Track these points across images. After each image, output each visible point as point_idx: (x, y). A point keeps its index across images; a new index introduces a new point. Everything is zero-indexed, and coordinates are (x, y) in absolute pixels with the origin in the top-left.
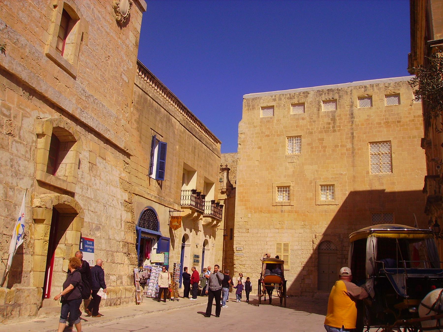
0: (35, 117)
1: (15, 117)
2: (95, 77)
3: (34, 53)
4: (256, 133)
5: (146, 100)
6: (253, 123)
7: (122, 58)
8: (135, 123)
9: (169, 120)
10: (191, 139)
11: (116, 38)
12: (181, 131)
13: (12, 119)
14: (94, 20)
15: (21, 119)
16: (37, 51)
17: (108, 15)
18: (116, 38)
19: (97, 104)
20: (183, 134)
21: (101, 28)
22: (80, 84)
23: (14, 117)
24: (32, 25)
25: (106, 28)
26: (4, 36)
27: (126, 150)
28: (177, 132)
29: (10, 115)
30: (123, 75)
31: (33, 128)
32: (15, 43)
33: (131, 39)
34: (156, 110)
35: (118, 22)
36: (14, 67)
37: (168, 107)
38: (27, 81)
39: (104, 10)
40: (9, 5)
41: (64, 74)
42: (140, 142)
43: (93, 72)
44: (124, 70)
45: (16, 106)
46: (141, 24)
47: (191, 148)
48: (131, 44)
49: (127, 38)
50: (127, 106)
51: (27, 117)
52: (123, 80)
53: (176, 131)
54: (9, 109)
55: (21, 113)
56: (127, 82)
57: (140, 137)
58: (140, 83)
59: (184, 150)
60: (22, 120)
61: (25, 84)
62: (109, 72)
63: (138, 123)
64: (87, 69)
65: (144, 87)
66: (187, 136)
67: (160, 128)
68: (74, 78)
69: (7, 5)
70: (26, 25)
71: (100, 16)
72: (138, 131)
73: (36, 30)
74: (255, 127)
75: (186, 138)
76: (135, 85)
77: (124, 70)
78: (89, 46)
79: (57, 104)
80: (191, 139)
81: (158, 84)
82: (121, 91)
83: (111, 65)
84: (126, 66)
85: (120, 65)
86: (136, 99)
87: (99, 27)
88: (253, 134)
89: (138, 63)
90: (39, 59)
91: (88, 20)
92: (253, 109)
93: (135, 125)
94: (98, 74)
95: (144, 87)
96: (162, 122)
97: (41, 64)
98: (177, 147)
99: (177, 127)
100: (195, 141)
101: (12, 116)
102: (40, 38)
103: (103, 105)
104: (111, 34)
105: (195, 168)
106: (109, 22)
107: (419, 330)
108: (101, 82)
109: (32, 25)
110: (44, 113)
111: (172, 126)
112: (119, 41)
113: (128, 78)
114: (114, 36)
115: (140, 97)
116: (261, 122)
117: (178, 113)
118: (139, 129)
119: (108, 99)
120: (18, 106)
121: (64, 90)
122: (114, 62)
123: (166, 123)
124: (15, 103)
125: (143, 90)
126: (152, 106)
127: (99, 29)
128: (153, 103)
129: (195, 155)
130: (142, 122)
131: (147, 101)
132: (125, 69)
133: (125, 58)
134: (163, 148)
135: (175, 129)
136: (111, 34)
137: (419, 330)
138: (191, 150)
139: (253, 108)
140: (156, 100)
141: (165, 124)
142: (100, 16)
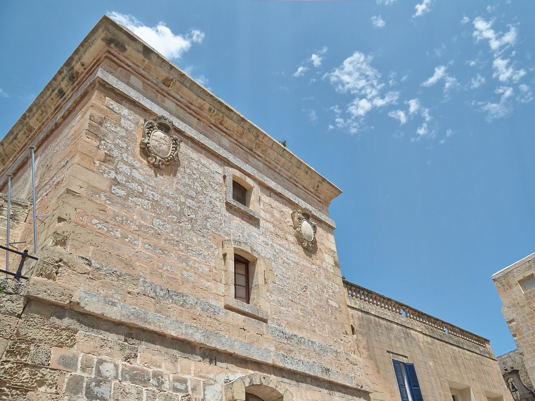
0: (222, 382)
1: (193, 389)
2: (294, 314)
3: (208, 309)
4: (528, 314)
5: (370, 321)
6: (518, 303)
7: (322, 284)
8: (364, 351)
9: (408, 335)
10: (446, 348)
11: (309, 265)
12: (428, 342)
13: (190, 393)
14: (276, 255)
15: (202, 389)
16: (210, 305)
17: (291, 245)
18: (309, 265)
19: (304, 343)
20: (432, 345)
21: (287, 261)
22: (277, 327)
23: (192, 389)
24: (202, 281)
25: (293, 259)
26: (167, 302)
27: (359, 388)
28: (424, 346)
29: (187, 388)
30: (330, 301)
31: (220, 396)
32: (182, 306)
33: (327, 260)
34: (386, 328)
35: (306, 249)
36: (184, 331)
37: (400, 320)
38: (203, 342)
39: (285, 242)
40: (169, 269)
41: (251, 321)
42: (379, 372)
43: (290, 309)
44: (329, 296)
45: (193, 375)
46: (334, 242)
47: (449, 359)
48: (329, 266)
49: (323, 261)
50: (347, 334)
51: (211, 385)
52: (331, 306)
53: (421, 345)
54: (184, 381)
55: (202, 383)
56: (338, 306)
57: (377, 366)
58: (355, 304)
59: (442, 364)
60: (204, 390)
61: (202, 346)
62: (311, 303)
63: (368, 349)
64: (282, 308)
65: (362, 306)
66: (439, 347)
67: (401, 347)
68: (265, 321)
69: (167, 270)
70: (193, 283)
71: (282, 249)
72: (372, 359)
73: (207, 285)
74: (522, 307)
75: (439, 349)
76: (349, 309)
77: (329, 296)
78: (277, 283)
79: (250, 358)
80: (446, 348)
81: (378, 298)
82: (333, 319)
83: (311, 295)
84: (330, 291)
85: (323, 292)
86: (356, 323)
87: (284, 260)
88: (524, 317)
89: (347, 284)
90: (216, 314)
91: (269, 257)
92: (510, 287)
93: (365, 353)
94: (297, 309)
95: (362, 306)
96: (399, 340)
97: (219, 319)
98: (431, 364)
99: (421, 340)
100: (452, 349)
101: (190, 389)
102: (214, 292)
103: (312, 342)
104: (302, 263)
105: (467, 383)
106: (295, 252)
107: (420, 8)
108: (304, 317)
109: (202, 281)
110: (234, 373)
111: (415, 339)
112: (313, 266)
113: (337, 302)
114: (305, 264)
115: (360, 319)
116: (527, 299)
117: (416, 323)
118: (371, 357)
119: (319, 333)
120: (197, 375)
121: (256, 340)
122: (314, 290)
123: (405, 338)
124: (192, 372)
125: (362, 311)
126: (380, 325)
127: (284, 262)
128: (379, 321)
129: (459, 367)
130: (373, 347)
131: (371, 321)
132: (331, 294)
133: (327, 283)
134: (410, 370)
135: (419, 342)
136: (302, 263)
137: (420, 8)
138: (451, 362)
139: (511, 287)
140: (382, 317)
141: (403, 341)
142: (282, 249)
